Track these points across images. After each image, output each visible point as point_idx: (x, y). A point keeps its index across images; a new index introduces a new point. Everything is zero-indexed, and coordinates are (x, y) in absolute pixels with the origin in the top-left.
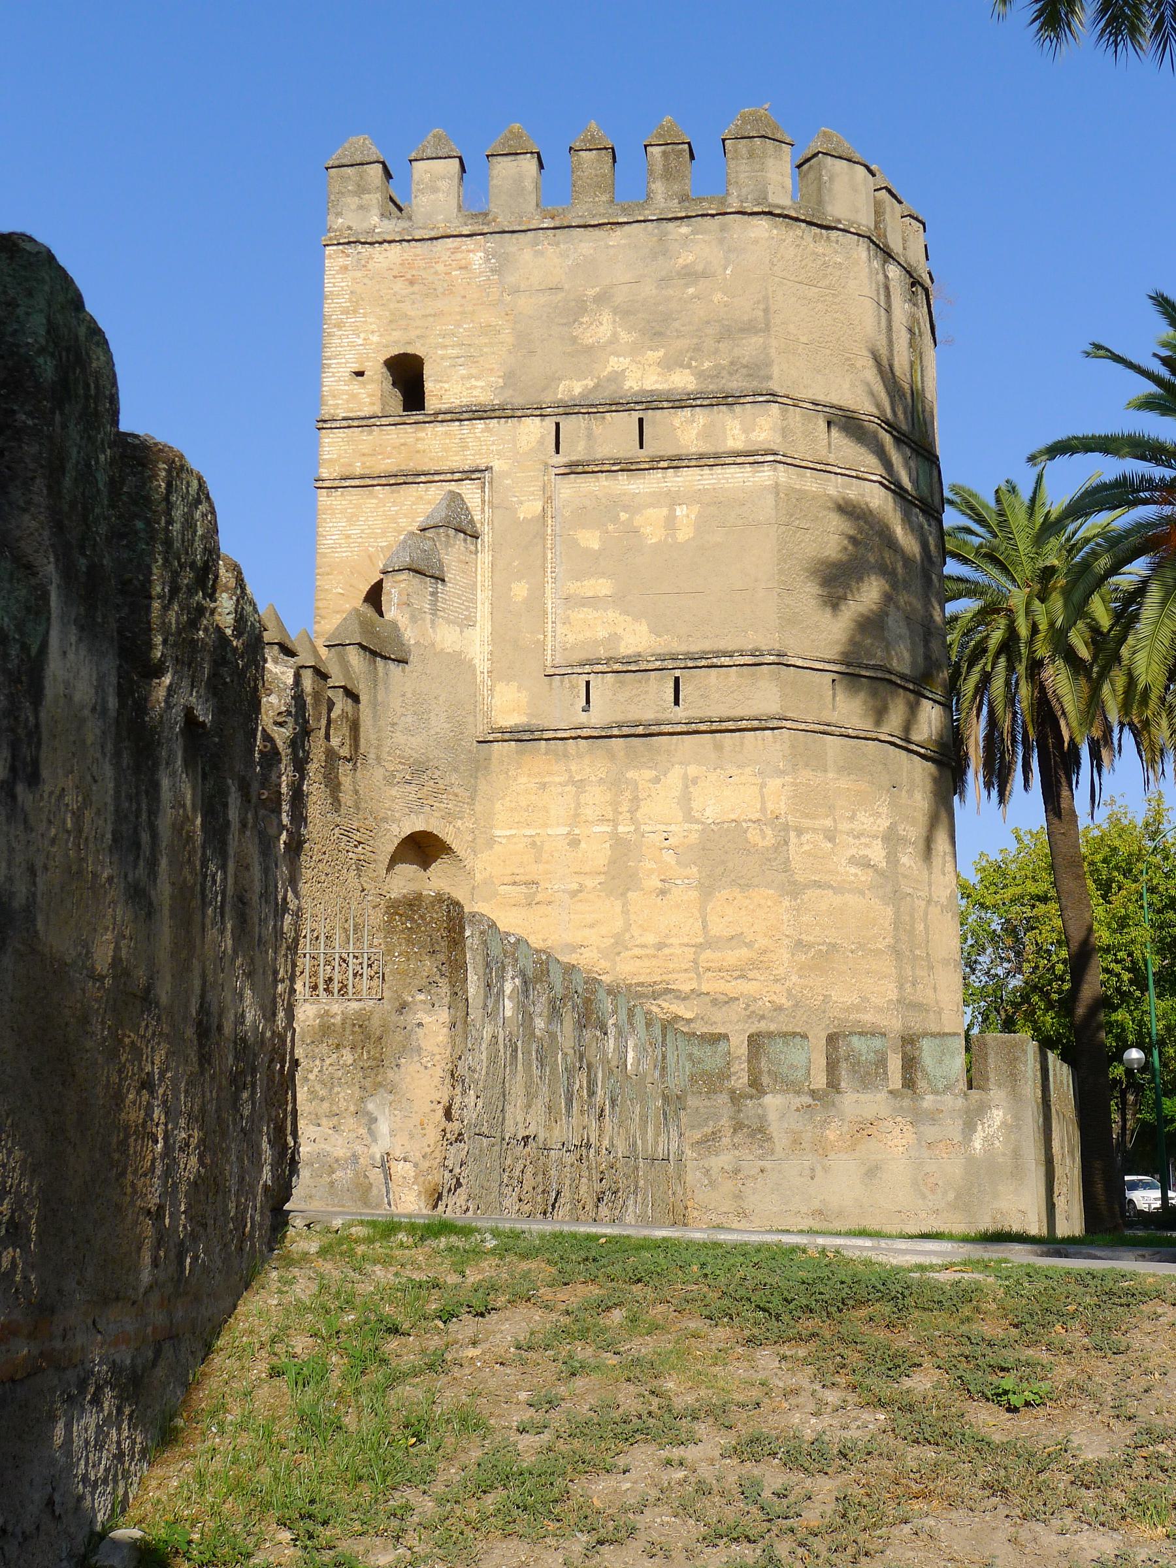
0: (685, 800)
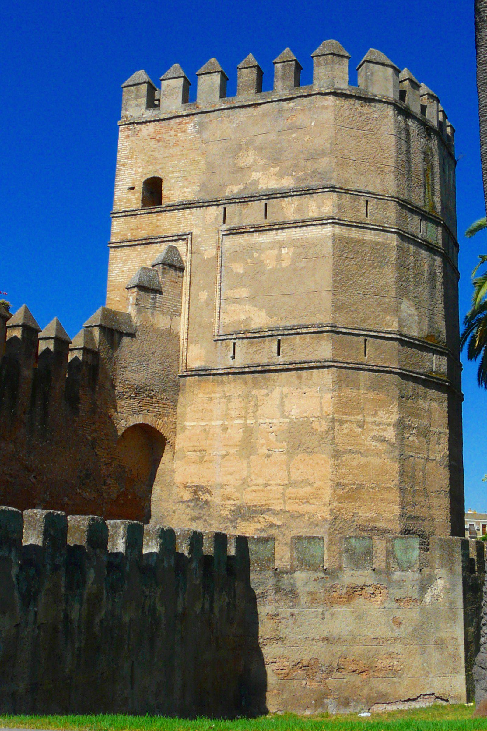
0: (282, 405)
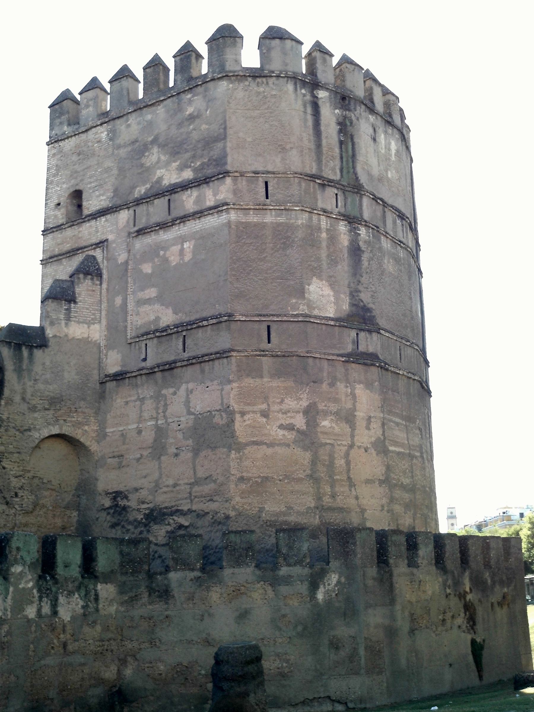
0: (187, 402)
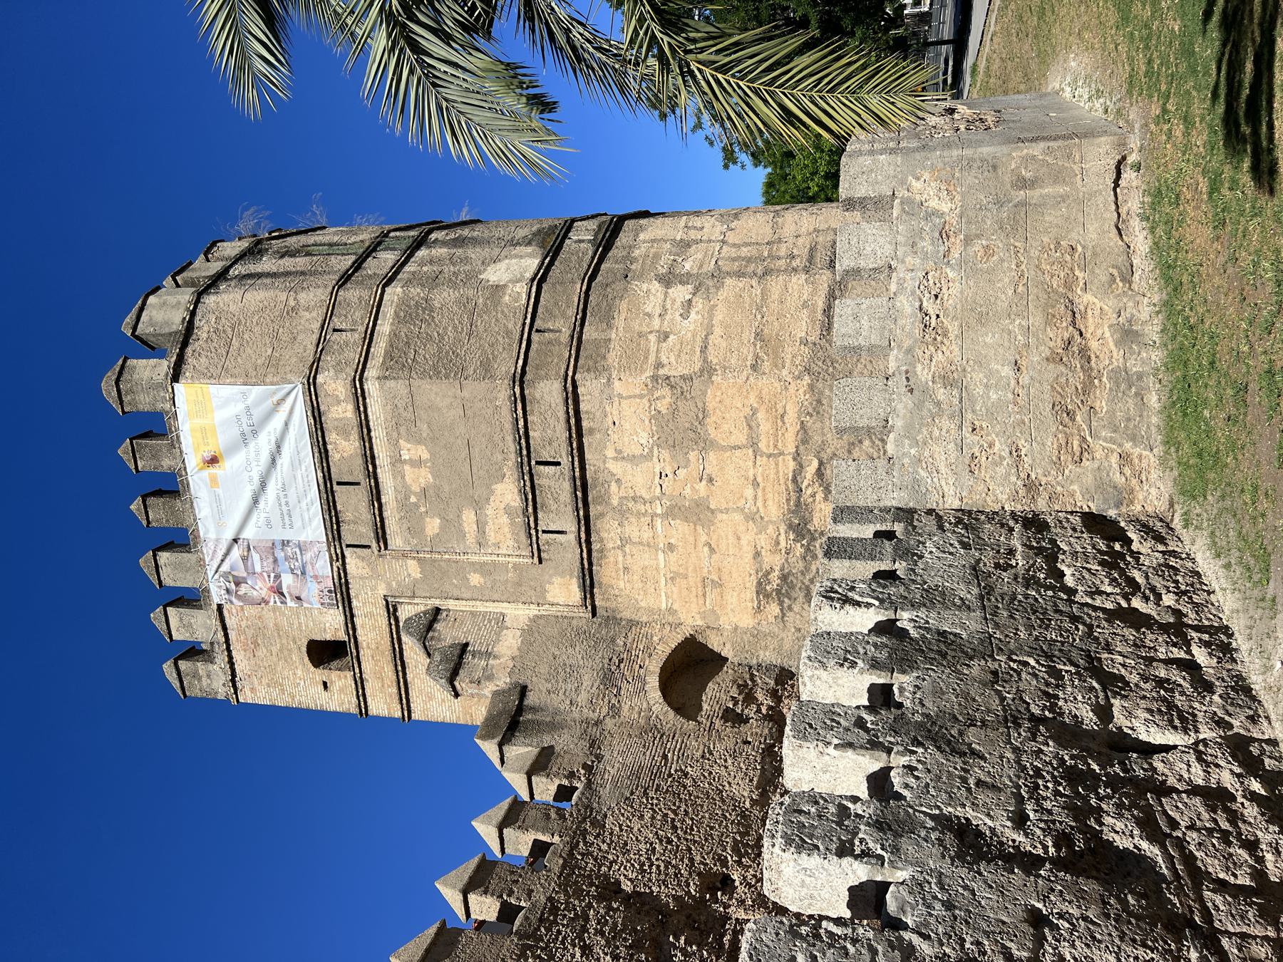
0: (632, 459)
